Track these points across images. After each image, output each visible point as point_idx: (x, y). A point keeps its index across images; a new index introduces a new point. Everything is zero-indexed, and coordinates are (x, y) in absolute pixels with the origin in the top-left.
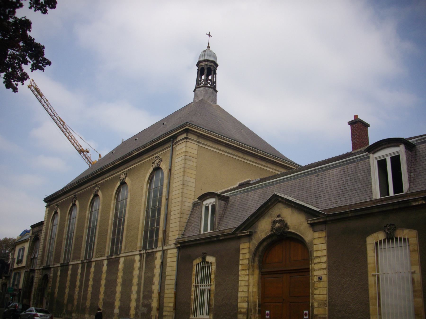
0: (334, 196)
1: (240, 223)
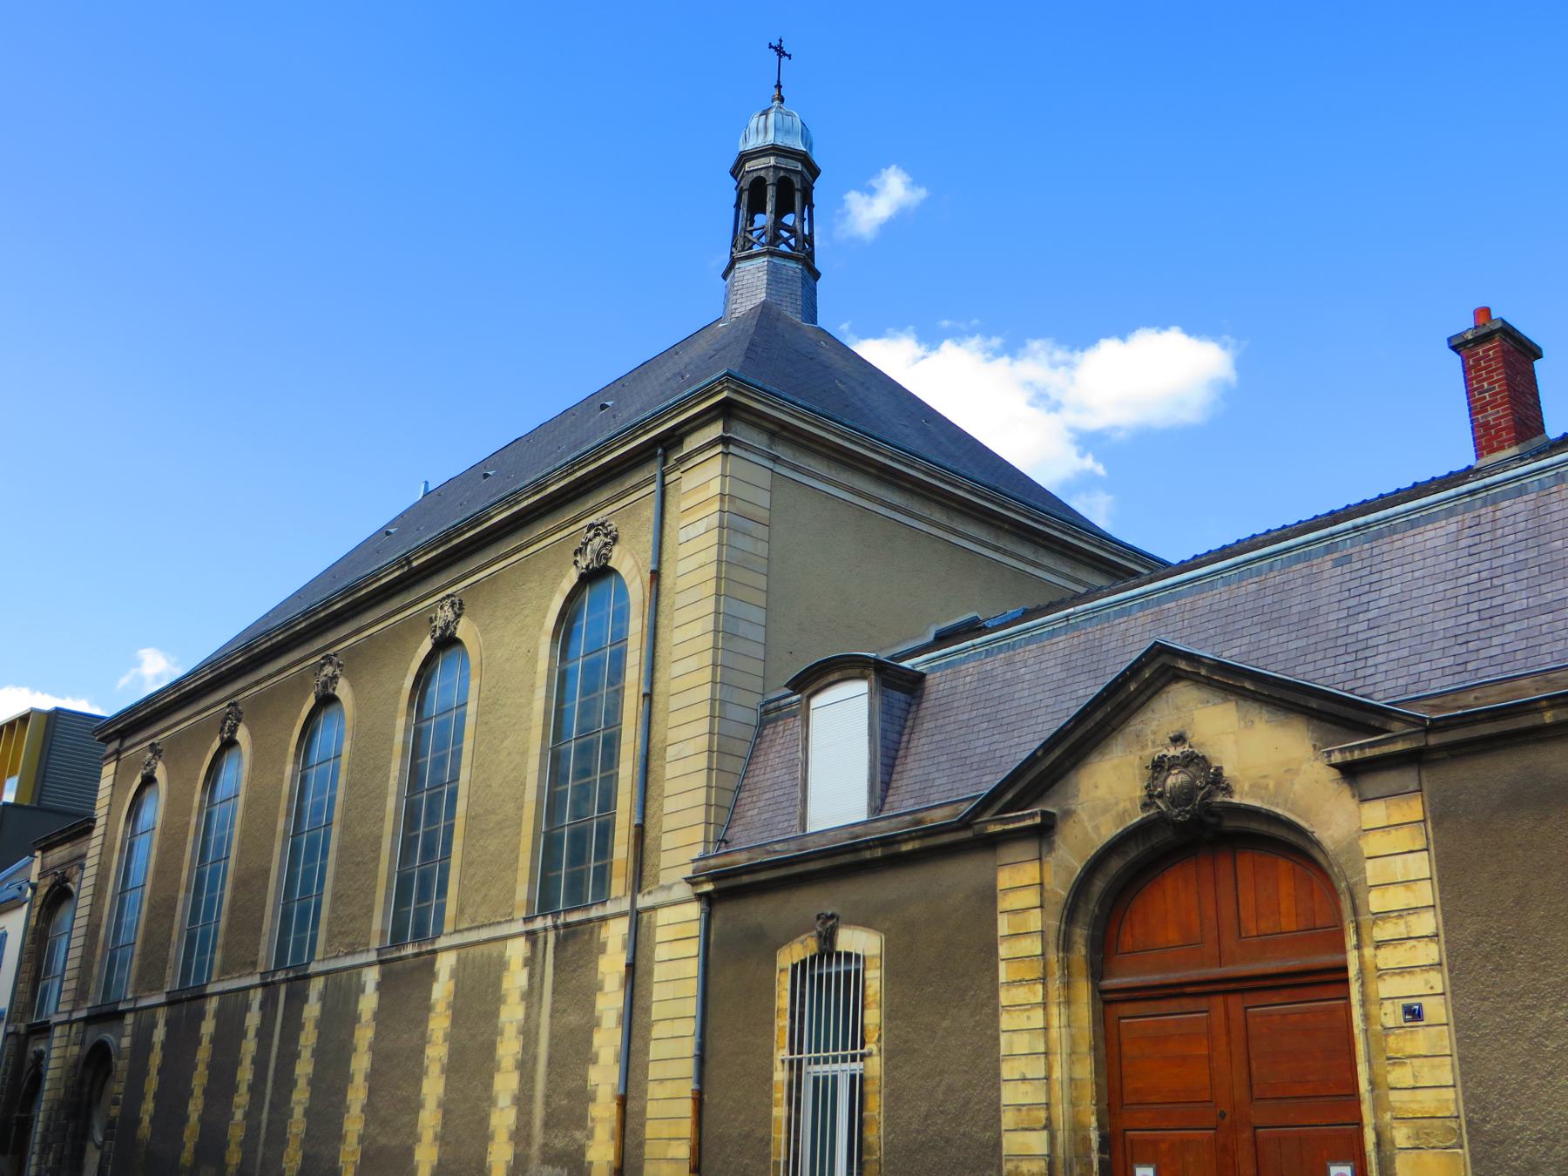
0: (1442, 644)
1: (1002, 776)
